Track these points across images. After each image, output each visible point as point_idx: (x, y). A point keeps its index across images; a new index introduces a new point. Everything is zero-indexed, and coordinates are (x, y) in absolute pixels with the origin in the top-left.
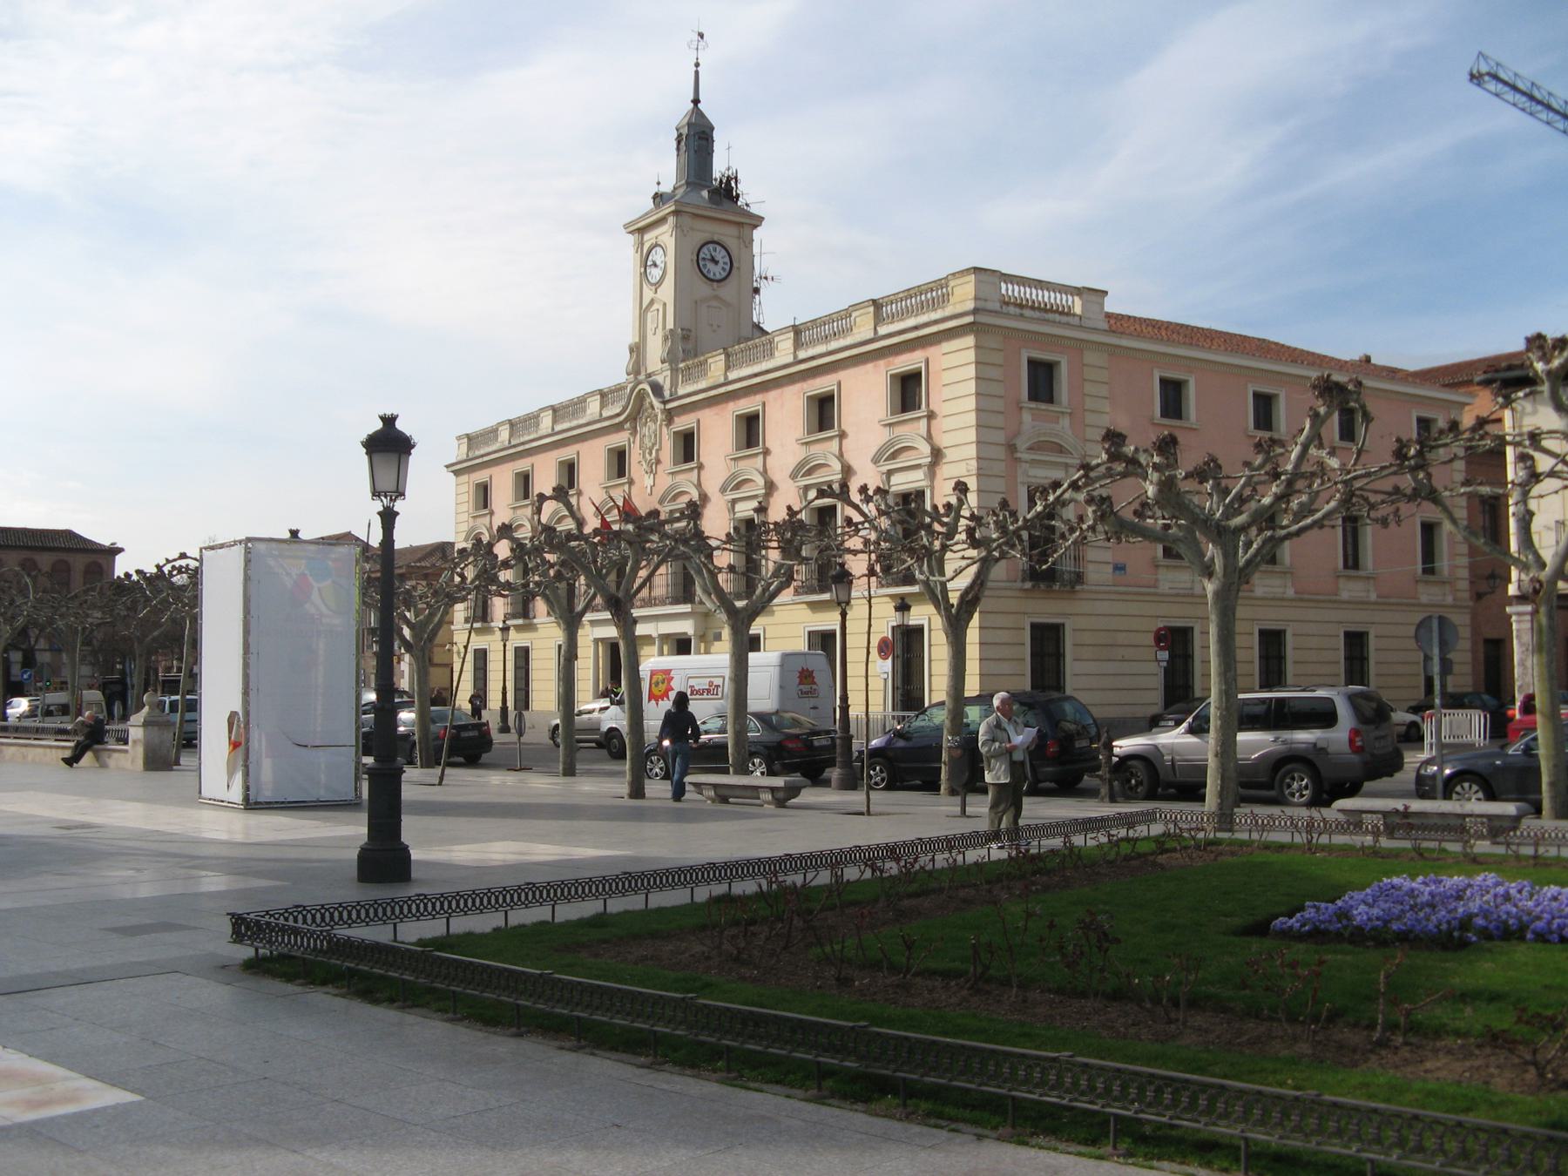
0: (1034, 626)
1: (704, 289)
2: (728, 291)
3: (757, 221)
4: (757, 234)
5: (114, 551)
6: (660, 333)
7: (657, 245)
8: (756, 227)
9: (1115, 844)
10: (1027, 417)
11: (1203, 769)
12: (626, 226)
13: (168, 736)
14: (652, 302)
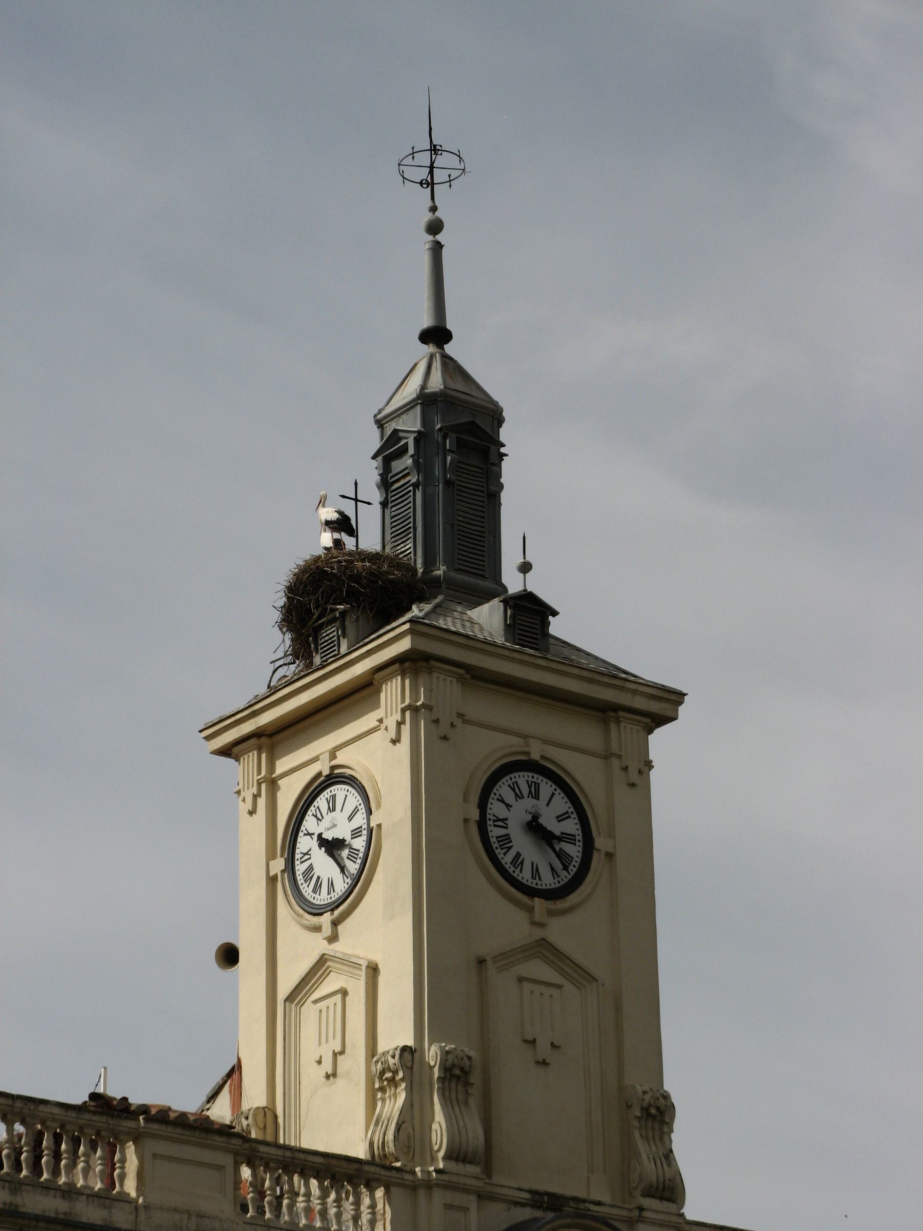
1: (504, 922)
2: (576, 929)
3: (638, 708)
4: (660, 742)
5: (503, 445)
6: (355, 1063)
7: (334, 778)
8: (662, 720)
12: (213, 729)
14: (321, 966)
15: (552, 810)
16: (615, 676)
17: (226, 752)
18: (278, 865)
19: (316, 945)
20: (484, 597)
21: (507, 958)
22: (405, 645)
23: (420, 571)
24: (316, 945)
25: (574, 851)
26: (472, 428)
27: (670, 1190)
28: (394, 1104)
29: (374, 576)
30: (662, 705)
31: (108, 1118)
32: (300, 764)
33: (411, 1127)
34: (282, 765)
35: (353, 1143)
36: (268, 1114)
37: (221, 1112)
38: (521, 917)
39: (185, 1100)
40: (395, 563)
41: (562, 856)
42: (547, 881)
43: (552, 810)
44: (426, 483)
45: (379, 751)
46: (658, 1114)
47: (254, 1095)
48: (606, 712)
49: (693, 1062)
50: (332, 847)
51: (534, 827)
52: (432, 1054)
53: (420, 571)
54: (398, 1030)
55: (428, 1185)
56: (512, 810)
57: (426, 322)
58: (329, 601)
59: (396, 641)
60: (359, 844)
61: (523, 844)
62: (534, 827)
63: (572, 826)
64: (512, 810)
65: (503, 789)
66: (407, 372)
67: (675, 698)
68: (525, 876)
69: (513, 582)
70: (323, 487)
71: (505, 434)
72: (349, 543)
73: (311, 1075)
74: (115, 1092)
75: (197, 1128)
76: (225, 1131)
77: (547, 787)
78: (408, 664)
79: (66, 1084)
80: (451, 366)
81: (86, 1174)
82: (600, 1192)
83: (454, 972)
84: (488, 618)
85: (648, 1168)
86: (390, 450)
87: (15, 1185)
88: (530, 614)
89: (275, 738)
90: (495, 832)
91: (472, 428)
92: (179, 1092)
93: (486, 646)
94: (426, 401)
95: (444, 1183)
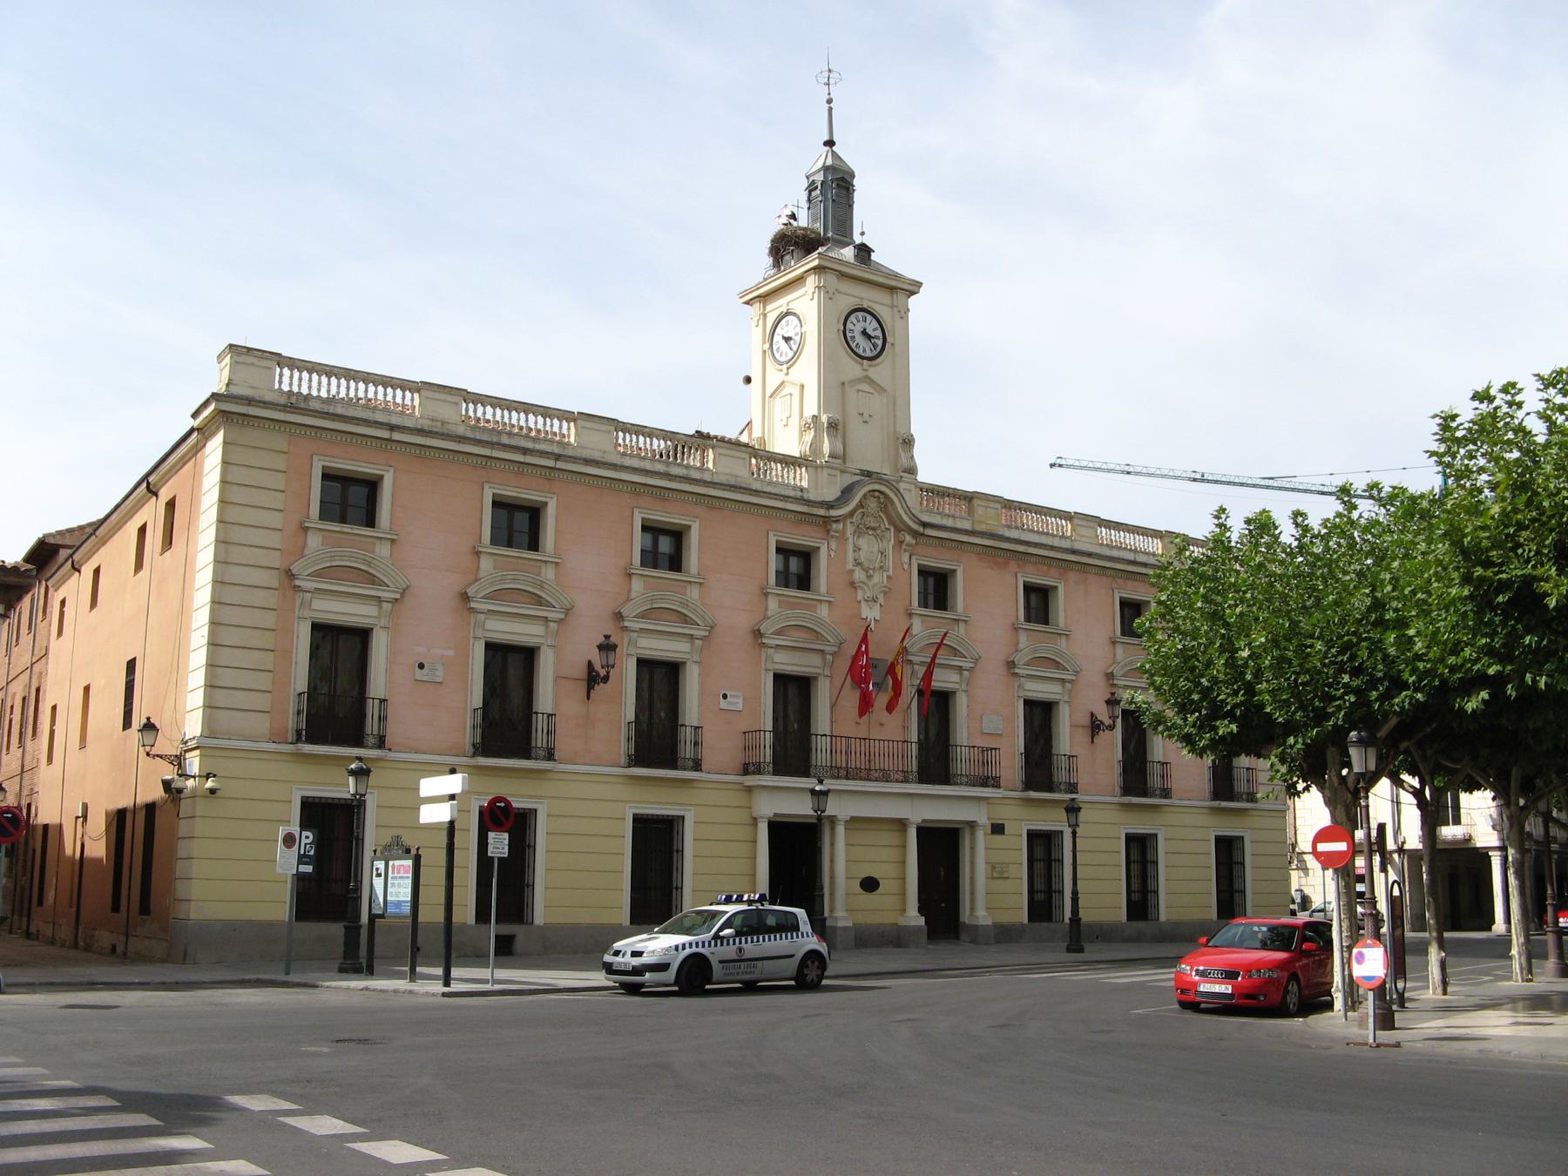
0: (637, 819)
1: (853, 369)
2: (879, 372)
3: (902, 288)
4: (912, 301)
6: (795, 422)
7: (788, 314)
8: (913, 293)
9: (1433, 893)
10: (773, 604)
11: (496, 954)
13: (1286, 974)
15: (872, 327)
16: (896, 276)
17: (747, 303)
18: (767, 346)
19: (781, 377)
20: (848, 244)
21: (853, 382)
22: (816, 263)
23: (820, 232)
24: (781, 377)
25: (880, 343)
26: (843, 179)
27: (912, 470)
28: (809, 436)
29: (804, 236)
30: (913, 288)
31: (702, 439)
32: (776, 307)
33: (815, 446)
34: (768, 308)
35: (794, 451)
36: (762, 440)
37: (744, 439)
38: (858, 367)
39: (731, 434)
40: (813, 231)
41: (875, 346)
42: (868, 354)
43: (872, 327)
44: (825, 201)
45: (806, 303)
46: (908, 442)
47: (757, 433)
48: (892, 289)
49: (920, 426)
50: (787, 339)
51: (864, 333)
52: (824, 418)
53: (820, 232)
54: (811, 408)
55: (822, 467)
56: (856, 326)
57: (826, 138)
58: (789, 244)
59: (813, 260)
60: (798, 338)
61: (860, 339)
62: (864, 333)
63: (879, 333)
64: (856, 326)
65: (852, 318)
66: (818, 158)
67: (919, 284)
68: (860, 352)
69: (858, 239)
70: (787, 201)
71: (855, 182)
72: (795, 224)
73: (778, 425)
74: (705, 431)
75: (737, 444)
76: (746, 445)
77: (869, 318)
78: (818, 270)
79: (686, 427)
80: (834, 154)
81: (694, 460)
82: (886, 470)
83: (834, 388)
84: (848, 253)
85: (904, 462)
86: (811, 188)
87: (668, 464)
88: (864, 252)
89: (765, 298)
90: (849, 335)
91: (843, 179)
92: (727, 429)
93: (847, 264)
94: (826, 169)
95: (828, 466)
